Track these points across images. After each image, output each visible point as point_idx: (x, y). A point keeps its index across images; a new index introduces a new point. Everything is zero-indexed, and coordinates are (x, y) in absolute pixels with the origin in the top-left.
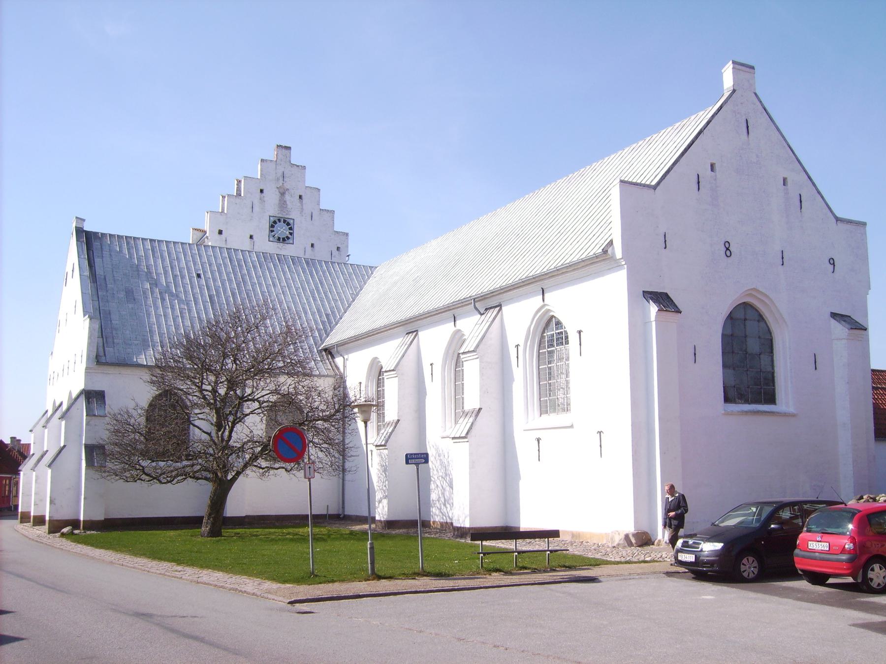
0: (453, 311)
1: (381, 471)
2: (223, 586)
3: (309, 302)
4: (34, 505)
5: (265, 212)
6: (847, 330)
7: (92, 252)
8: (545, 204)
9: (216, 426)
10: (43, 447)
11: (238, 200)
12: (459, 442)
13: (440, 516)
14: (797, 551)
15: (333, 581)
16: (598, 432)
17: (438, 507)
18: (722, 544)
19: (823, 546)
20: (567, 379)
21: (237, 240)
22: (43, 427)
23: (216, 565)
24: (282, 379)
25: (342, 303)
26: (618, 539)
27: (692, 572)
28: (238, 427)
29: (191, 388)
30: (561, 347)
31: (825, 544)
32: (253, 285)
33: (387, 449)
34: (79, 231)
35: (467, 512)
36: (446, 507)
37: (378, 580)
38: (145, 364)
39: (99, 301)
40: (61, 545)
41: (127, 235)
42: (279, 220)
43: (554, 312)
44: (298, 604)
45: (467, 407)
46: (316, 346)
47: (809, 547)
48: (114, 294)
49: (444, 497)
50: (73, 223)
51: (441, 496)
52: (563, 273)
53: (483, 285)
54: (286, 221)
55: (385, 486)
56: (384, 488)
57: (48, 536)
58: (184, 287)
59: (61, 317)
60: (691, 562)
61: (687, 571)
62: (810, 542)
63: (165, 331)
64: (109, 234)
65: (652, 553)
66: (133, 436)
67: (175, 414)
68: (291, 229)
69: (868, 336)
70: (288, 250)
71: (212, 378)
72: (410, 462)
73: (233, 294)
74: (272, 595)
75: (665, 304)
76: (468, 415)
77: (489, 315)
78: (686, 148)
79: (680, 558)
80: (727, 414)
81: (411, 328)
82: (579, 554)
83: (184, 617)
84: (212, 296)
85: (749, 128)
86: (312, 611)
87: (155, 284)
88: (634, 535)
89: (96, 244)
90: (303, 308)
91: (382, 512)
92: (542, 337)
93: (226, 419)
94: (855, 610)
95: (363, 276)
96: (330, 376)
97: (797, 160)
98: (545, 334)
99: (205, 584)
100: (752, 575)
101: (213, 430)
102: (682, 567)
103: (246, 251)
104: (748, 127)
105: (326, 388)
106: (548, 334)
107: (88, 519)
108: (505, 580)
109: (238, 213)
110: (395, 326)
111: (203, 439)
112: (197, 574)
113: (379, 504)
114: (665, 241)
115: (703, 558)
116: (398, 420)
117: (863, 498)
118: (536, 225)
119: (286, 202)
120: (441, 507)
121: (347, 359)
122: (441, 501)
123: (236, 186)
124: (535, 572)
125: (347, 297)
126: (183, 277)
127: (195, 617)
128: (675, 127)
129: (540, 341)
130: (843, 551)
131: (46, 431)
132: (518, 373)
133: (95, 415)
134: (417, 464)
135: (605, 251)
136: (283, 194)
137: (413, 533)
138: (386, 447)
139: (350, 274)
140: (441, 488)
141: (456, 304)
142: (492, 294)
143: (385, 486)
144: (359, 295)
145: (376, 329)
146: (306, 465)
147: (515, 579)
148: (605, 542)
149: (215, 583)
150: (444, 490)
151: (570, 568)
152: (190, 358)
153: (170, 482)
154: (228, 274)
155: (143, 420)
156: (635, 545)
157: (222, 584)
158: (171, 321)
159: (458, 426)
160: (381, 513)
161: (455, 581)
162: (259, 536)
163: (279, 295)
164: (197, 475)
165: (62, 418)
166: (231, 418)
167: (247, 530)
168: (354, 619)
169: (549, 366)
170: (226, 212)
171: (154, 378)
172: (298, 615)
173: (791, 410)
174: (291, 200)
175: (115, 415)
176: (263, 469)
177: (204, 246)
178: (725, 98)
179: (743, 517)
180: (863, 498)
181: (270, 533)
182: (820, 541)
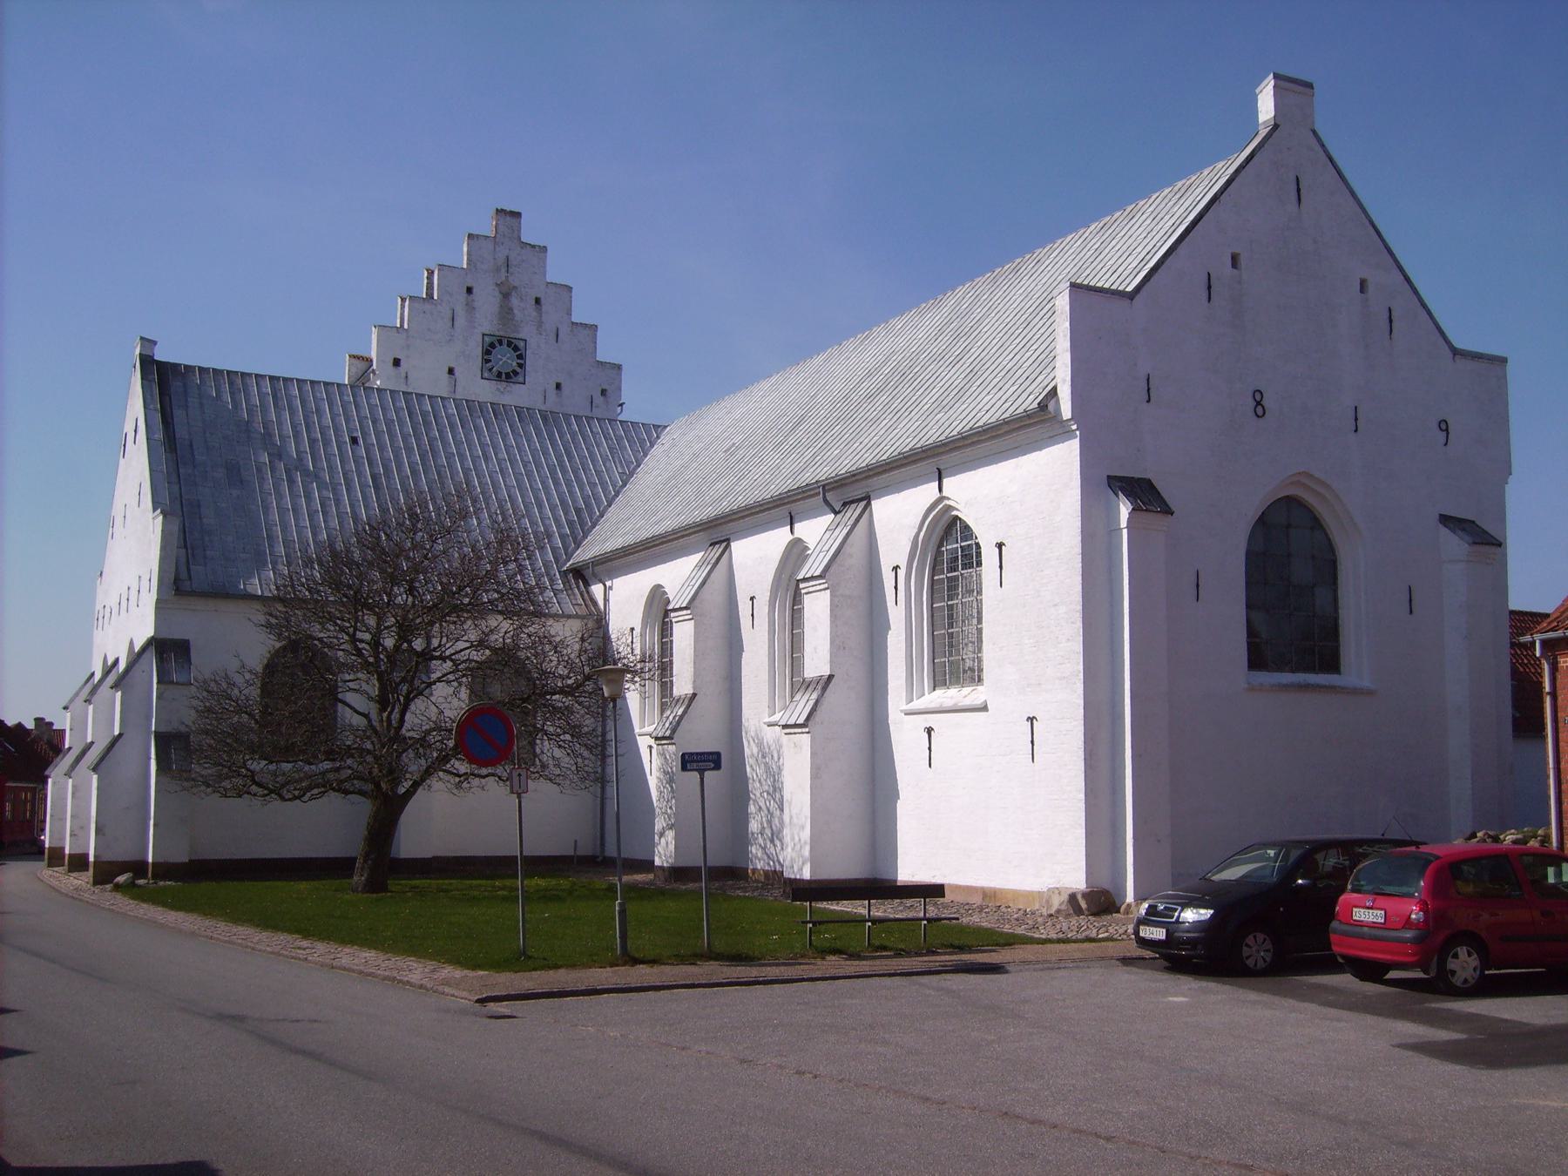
0: (789, 506)
1: (665, 782)
2: (373, 973)
3: (546, 487)
4: (71, 835)
5: (475, 327)
6: (1467, 545)
7: (168, 398)
8: (951, 321)
9: (378, 702)
10: (86, 738)
11: (427, 307)
12: (795, 733)
13: (764, 860)
14: (1334, 924)
15: (556, 967)
16: (1029, 718)
17: (760, 845)
18: (1212, 912)
19: (1376, 916)
20: (979, 626)
21: (426, 377)
22: (85, 701)
23: (367, 939)
24: (493, 621)
25: (605, 490)
26: (1057, 902)
27: (1164, 957)
28: (418, 705)
29: (337, 638)
30: (969, 571)
31: (1379, 912)
32: (449, 456)
33: (674, 744)
34: (147, 362)
35: (806, 852)
36: (775, 846)
37: (632, 966)
38: (260, 593)
39: (180, 483)
40: (113, 904)
41: (229, 369)
42: (500, 343)
43: (957, 510)
44: (492, 1004)
45: (677, 692)
46: (557, 563)
47: (1354, 918)
48: (206, 472)
49: (771, 827)
50: (135, 348)
51: (765, 825)
52: (973, 443)
53: (840, 461)
54: (487, 349)
55: (671, 808)
56: (669, 811)
57: (93, 889)
58: (328, 461)
59: (117, 511)
60: (1160, 941)
61: (1157, 956)
62: (1355, 910)
63: (294, 537)
64: (199, 367)
65: (1110, 925)
66: (236, 719)
67: (308, 682)
68: (520, 357)
69: (1505, 555)
70: (515, 396)
71: (372, 621)
72: (689, 768)
73: (414, 472)
74: (450, 989)
75: (1146, 500)
76: (810, 688)
77: (848, 514)
78: (1188, 226)
79: (1142, 934)
80: (1251, 688)
81: (717, 536)
82: (989, 926)
83: (298, 1021)
84: (378, 476)
85: (1302, 191)
86: (515, 1014)
87: (278, 454)
88: (1085, 895)
89: (176, 385)
90: (536, 498)
91: (665, 852)
92: (938, 553)
93: (395, 690)
94: (1414, 1021)
95: (642, 442)
96: (577, 616)
97: (1386, 248)
98: (944, 549)
99: (345, 969)
100: (1261, 964)
101: (372, 709)
102: (1148, 950)
103: (437, 397)
104: (1299, 190)
105: (568, 639)
106: (948, 547)
107: (162, 861)
108: (847, 967)
109: (429, 330)
110: (691, 531)
111: (354, 723)
112: (334, 953)
113: (660, 839)
114: (1149, 390)
115: (1181, 934)
116: (694, 695)
117: (1476, 837)
118: (935, 357)
119: (512, 310)
120: (765, 844)
121: (611, 588)
122: (767, 835)
123: (425, 281)
124: (900, 954)
125: (613, 478)
126: (327, 443)
127: (315, 1021)
128: (1176, 189)
129: (935, 559)
130: (1408, 923)
131: (91, 707)
132: (896, 614)
133: (172, 682)
134: (701, 772)
135: (1043, 406)
136: (506, 296)
137: (716, 889)
138: (673, 741)
139: (619, 439)
140: (766, 812)
141: (794, 495)
142: (854, 479)
143: (671, 808)
144: (635, 476)
145: (661, 536)
146: (514, 771)
147: (864, 966)
148: (1037, 907)
149: (362, 968)
150: (772, 815)
151: (961, 949)
152: (337, 585)
153: (299, 798)
154: (405, 438)
155: (254, 692)
156: (1086, 913)
157: (371, 970)
158: (304, 520)
159: (793, 705)
160: (662, 852)
161: (760, 968)
162: (452, 891)
163: (494, 475)
164: (347, 785)
165: (115, 686)
166: (405, 688)
167: (433, 882)
168: (580, 1027)
169: (949, 603)
170: (406, 326)
171: (273, 621)
172: (488, 1020)
173: (1366, 683)
174: (522, 308)
175: (205, 682)
176: (460, 776)
177: (364, 389)
178: (1260, 139)
179: (1256, 862)
180: (1476, 837)
181: (471, 887)
182: (1371, 908)
